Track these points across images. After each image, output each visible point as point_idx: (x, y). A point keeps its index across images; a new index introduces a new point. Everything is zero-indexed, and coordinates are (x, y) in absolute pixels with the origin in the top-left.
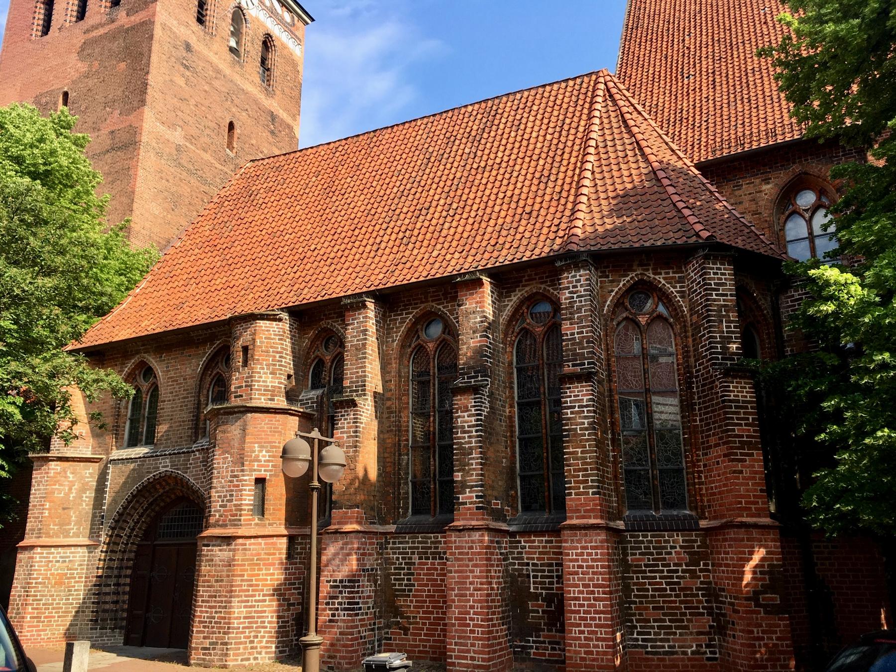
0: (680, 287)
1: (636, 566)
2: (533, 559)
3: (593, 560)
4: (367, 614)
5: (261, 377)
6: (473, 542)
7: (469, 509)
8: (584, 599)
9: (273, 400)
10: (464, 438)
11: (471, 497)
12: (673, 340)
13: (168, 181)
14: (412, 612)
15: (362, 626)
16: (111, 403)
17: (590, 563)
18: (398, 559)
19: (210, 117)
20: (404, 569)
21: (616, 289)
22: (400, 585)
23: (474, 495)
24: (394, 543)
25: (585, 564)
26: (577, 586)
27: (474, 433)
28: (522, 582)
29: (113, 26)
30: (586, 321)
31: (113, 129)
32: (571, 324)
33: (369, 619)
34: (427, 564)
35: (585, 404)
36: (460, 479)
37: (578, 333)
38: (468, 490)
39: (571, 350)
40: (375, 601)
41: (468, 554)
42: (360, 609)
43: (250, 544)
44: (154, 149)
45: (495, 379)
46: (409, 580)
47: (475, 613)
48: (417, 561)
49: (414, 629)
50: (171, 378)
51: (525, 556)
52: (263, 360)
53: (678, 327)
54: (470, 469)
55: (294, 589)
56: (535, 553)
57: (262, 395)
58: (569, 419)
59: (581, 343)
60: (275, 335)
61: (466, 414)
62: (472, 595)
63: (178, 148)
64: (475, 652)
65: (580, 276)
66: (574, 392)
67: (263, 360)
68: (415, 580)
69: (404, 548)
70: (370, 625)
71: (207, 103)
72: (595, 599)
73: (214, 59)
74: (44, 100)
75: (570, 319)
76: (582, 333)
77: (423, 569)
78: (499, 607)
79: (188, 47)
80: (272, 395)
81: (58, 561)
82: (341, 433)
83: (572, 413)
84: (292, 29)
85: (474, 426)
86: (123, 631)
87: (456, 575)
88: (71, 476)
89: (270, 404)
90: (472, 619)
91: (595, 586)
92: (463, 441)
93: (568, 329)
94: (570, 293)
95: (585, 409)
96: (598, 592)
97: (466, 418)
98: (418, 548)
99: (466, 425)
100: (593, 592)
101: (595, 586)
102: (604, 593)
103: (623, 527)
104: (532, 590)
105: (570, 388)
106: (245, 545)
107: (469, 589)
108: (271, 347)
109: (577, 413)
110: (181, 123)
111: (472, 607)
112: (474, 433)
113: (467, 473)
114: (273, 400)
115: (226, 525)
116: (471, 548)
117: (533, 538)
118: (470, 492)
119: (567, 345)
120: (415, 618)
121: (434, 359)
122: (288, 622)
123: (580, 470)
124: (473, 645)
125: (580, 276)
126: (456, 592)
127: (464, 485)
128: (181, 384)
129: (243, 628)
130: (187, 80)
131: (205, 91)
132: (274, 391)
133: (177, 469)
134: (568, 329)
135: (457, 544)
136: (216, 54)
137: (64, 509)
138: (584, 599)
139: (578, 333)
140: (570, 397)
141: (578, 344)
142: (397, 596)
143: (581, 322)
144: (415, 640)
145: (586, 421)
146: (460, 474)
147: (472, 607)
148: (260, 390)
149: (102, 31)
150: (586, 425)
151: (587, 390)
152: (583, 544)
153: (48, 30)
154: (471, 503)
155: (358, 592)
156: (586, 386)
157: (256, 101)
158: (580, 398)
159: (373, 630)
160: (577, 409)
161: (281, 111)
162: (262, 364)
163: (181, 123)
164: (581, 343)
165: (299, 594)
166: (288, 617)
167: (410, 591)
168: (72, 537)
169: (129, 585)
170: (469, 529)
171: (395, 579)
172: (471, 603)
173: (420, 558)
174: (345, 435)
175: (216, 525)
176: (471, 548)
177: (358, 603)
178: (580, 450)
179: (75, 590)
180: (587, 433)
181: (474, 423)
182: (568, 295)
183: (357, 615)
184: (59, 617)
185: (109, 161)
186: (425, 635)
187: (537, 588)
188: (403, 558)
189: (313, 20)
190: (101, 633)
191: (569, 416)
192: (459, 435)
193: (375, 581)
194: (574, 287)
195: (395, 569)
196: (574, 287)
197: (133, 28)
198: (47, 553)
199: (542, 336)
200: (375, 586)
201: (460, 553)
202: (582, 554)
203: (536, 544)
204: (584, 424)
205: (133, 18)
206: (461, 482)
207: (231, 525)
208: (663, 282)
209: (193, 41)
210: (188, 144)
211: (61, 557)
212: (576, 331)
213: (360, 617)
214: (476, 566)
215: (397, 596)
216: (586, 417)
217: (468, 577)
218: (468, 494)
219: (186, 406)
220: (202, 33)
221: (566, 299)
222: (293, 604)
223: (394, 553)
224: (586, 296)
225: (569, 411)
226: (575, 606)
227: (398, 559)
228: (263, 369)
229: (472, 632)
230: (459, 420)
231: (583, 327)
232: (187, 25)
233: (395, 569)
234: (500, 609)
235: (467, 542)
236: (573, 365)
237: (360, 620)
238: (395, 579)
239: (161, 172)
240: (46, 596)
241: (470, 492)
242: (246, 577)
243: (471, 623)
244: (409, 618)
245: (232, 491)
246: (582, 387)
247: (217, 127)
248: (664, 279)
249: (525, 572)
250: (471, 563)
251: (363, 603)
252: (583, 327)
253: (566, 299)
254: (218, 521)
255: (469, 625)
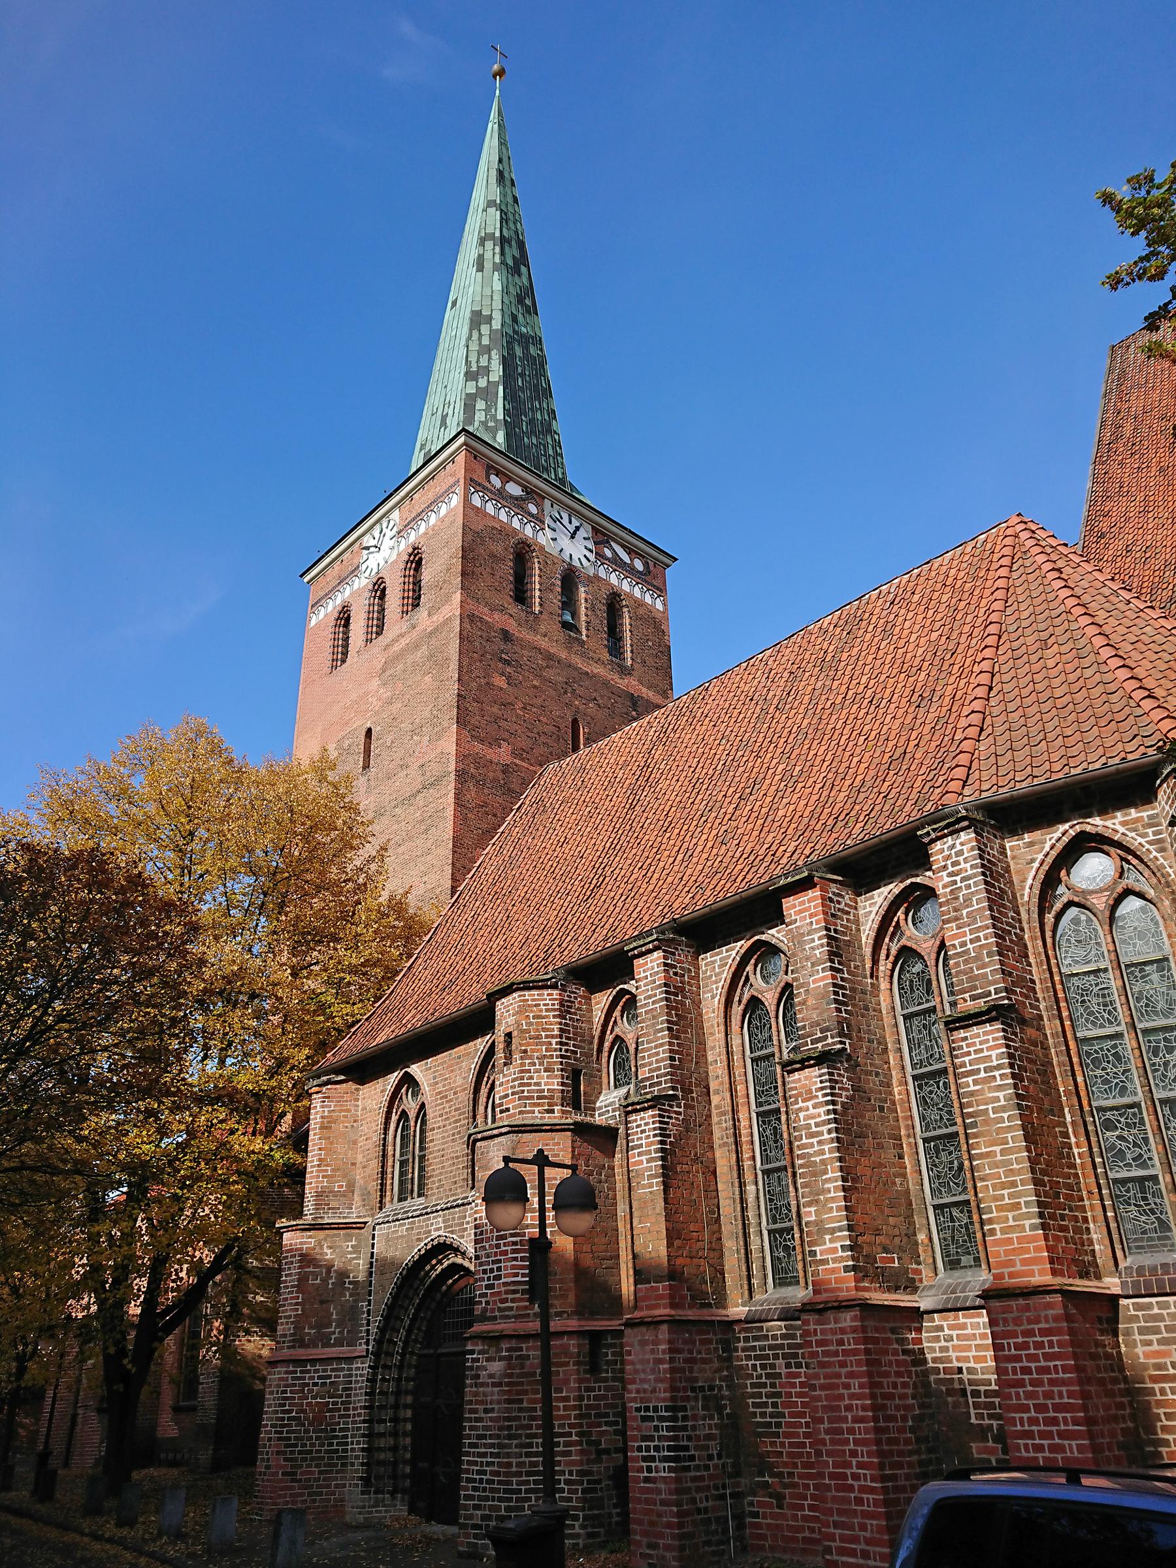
0: (1155, 834)
1: (1159, 1367)
2: (967, 1359)
3: (1048, 1357)
4: (707, 1467)
5: (531, 1078)
6: (843, 1331)
7: (833, 1271)
8: (1043, 1435)
9: (552, 1111)
10: (812, 1145)
11: (835, 1250)
12: (1162, 928)
13: (495, 815)
14: (786, 1465)
15: (698, 1489)
16: (375, 1139)
17: (1043, 1364)
18: (754, 1367)
19: (544, 720)
20: (764, 1385)
21: (1040, 857)
22: (763, 1415)
23: (838, 1245)
24: (746, 1339)
25: (1033, 1365)
26: (1026, 1409)
27: (826, 1136)
28: (956, 1405)
29: (415, 634)
30: (982, 919)
31: (421, 761)
32: (959, 928)
33: (711, 1477)
34: (798, 1375)
35: (995, 1063)
36: (813, 1218)
37: (972, 941)
38: (828, 1237)
39: (964, 972)
40: (721, 1444)
41: (836, 1354)
42: (692, 1458)
43: (528, 1349)
44: (473, 776)
45: (860, 1039)
46: (775, 1405)
47: (860, 1465)
48: (784, 1371)
49: (793, 1496)
50: (440, 1093)
51: (953, 1354)
52: (533, 1051)
53: (1167, 903)
54: (827, 1200)
55: (607, 1424)
56: (969, 1348)
57: (535, 1105)
58: (972, 1094)
59: (978, 958)
60: (547, 1010)
61: (810, 1104)
62: (851, 1431)
63: (506, 770)
64: (868, 1542)
65: (962, 844)
66: (974, 1044)
67: (533, 1051)
68: (784, 1405)
69: (762, 1348)
70: (717, 1488)
71: (539, 701)
72: (1062, 1435)
73: (544, 643)
74: (345, 746)
75: (956, 919)
76: (978, 939)
77: (793, 1385)
78: (911, 1453)
79: (506, 636)
80: (550, 1104)
81: (315, 1384)
82: (639, 1154)
83: (975, 1082)
84: (648, 578)
85: (824, 1123)
86: (406, 1497)
87: (823, 1393)
88: (329, 1251)
89: (548, 1119)
90: (856, 1477)
91: (1058, 1408)
92: (810, 1151)
93: (954, 937)
94: (949, 875)
95: (997, 1073)
96: (1066, 1423)
97: (812, 1111)
98: (781, 1347)
99: (812, 1122)
100: (1054, 1421)
101: (1058, 1408)
102: (1076, 1422)
103: (1117, 1290)
104: (973, 1421)
105: (966, 1038)
106: (521, 1349)
107: (845, 1420)
108: (544, 1030)
109: (984, 1081)
110: (506, 735)
111: (854, 1454)
112: (826, 1136)
113: (823, 1207)
114: (552, 1111)
115: (495, 1318)
116: (841, 1342)
117: (962, 1320)
118: (831, 1241)
119: (957, 964)
120: (791, 1475)
121: (777, 1017)
122: (599, 1482)
123: (1003, 1186)
124: (863, 1527)
125: (962, 844)
126: (826, 1425)
127: (821, 1228)
128: (451, 1100)
129: (527, 1491)
130: (509, 678)
131: (535, 687)
132: (552, 1097)
133: (452, 1232)
134: (954, 937)
135: (819, 1337)
136: (545, 636)
137: (322, 1302)
138: (1043, 1435)
139: (972, 941)
140: (969, 1054)
141: (977, 959)
142: (761, 1435)
143: (975, 921)
144: (795, 1518)
145: (1001, 1095)
146: (813, 1209)
147: (854, 1454)
148: (532, 1098)
149: (403, 642)
150: (1003, 1103)
151: (994, 1039)
152: (1026, 1327)
153: (345, 654)
154: (835, 1260)
155: (684, 1428)
156: (992, 1032)
157: (606, 684)
158: (986, 1053)
159: (722, 1497)
160: (983, 1075)
161: (644, 690)
162: (531, 1058)
163: (506, 735)
164: (978, 958)
165: (616, 1432)
166: (599, 1473)
167: (778, 1425)
168: (334, 1345)
169: (410, 1420)
170: (833, 1308)
171: (755, 1405)
172: (852, 1446)
173: (788, 1366)
174: (644, 1158)
175: (483, 1318)
176: (841, 1342)
177: (686, 1448)
178: (997, 1149)
179: (341, 1430)
180: (1005, 1115)
181: (824, 1118)
182: (947, 880)
183: (687, 1469)
184: (320, 1473)
185: (421, 803)
186: (812, 1508)
187: (980, 1416)
188: (763, 1367)
189: (676, 559)
190: (377, 1500)
191: (972, 1088)
192: (804, 1141)
193: (720, 1409)
194: (954, 864)
195: (753, 1385)
196: (954, 864)
197: (436, 629)
198: (301, 1372)
199: (933, 956)
200: (721, 1417)
201: (825, 1353)
202: (1025, 1346)
203: (969, 1331)
204: (997, 1099)
205: (435, 618)
206: (816, 1223)
207: (502, 1317)
208: (1122, 829)
209: (512, 626)
210: (517, 761)
211: (319, 1378)
212: (969, 937)
213: (692, 1474)
214: (851, 1375)
215: (761, 1435)
216: (1000, 1088)
217: (841, 1397)
218: (828, 1245)
219: (459, 1133)
220: (523, 615)
221: (944, 887)
222: (607, 1451)
223: (748, 1358)
224: (975, 876)
225: (970, 1079)
226: (1027, 1450)
227: (754, 1366)
228: (534, 1064)
229: (859, 1501)
230: (801, 1115)
231: (979, 929)
232: (503, 610)
233: (753, 1385)
234: (915, 1458)
235: (833, 1332)
236: (973, 998)
237: (695, 1479)
238: (755, 1405)
239: (486, 804)
240: (302, 1439)
241: (831, 1241)
242: (525, 1405)
243: (856, 1484)
244: (780, 1475)
245: (499, 1261)
246: (985, 1034)
247: (555, 730)
248: (1123, 824)
249: (957, 1386)
250: (843, 1370)
251: (696, 1448)
252: (979, 929)
253: (944, 887)
254: (485, 1310)
255: (851, 1488)
